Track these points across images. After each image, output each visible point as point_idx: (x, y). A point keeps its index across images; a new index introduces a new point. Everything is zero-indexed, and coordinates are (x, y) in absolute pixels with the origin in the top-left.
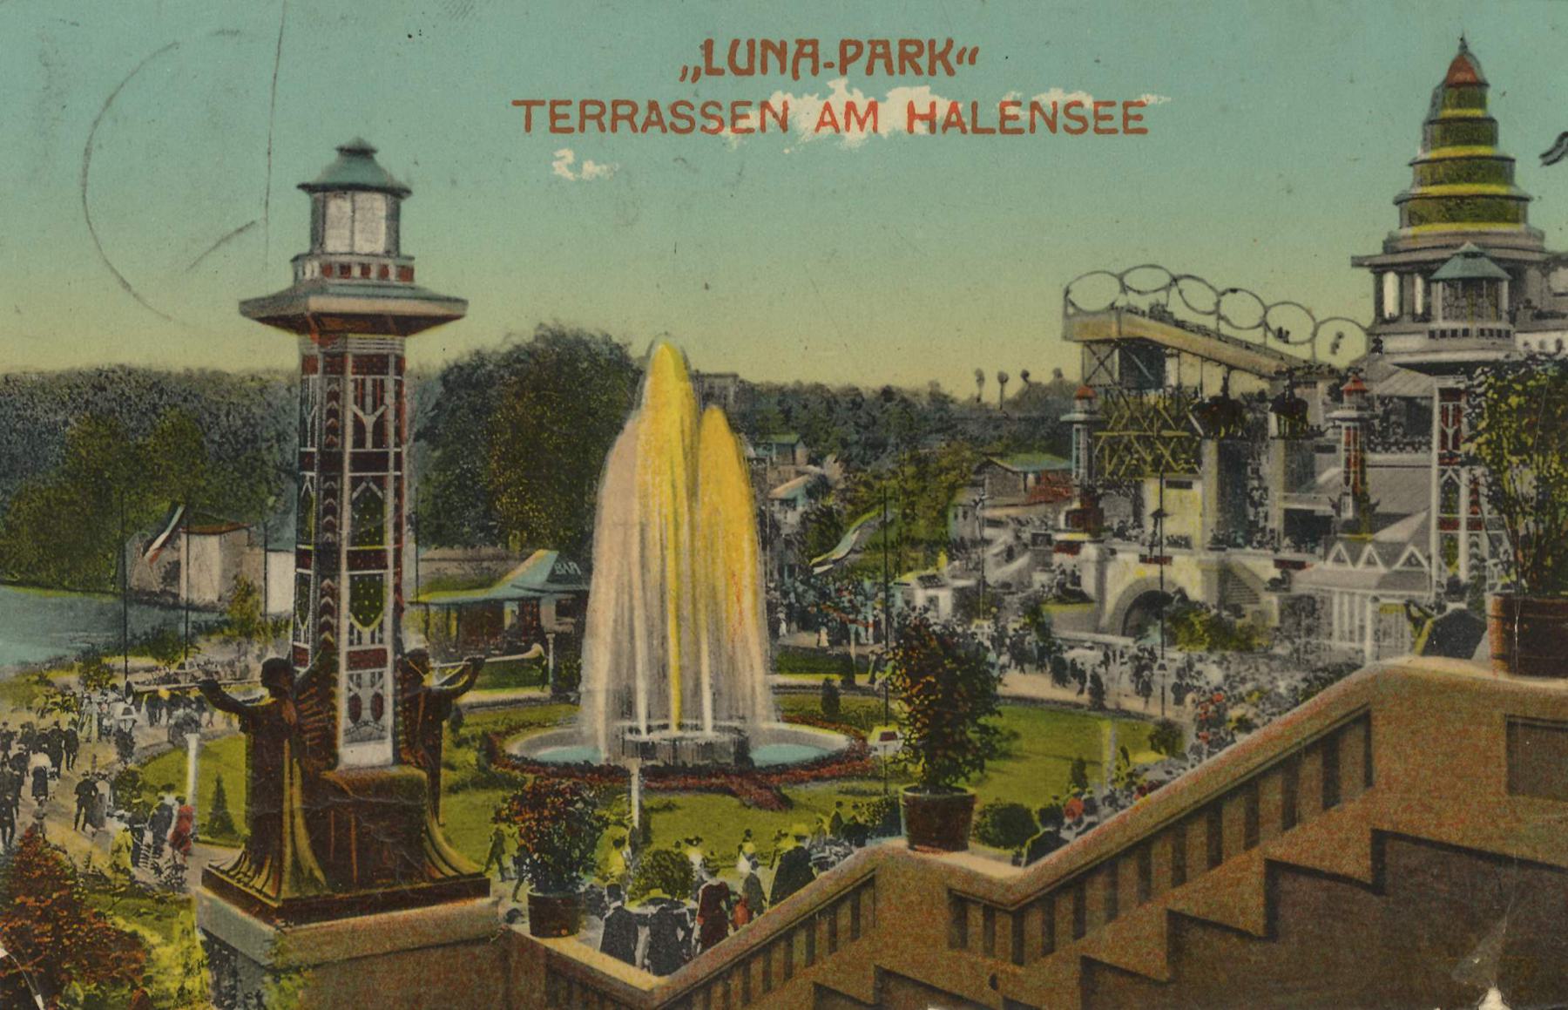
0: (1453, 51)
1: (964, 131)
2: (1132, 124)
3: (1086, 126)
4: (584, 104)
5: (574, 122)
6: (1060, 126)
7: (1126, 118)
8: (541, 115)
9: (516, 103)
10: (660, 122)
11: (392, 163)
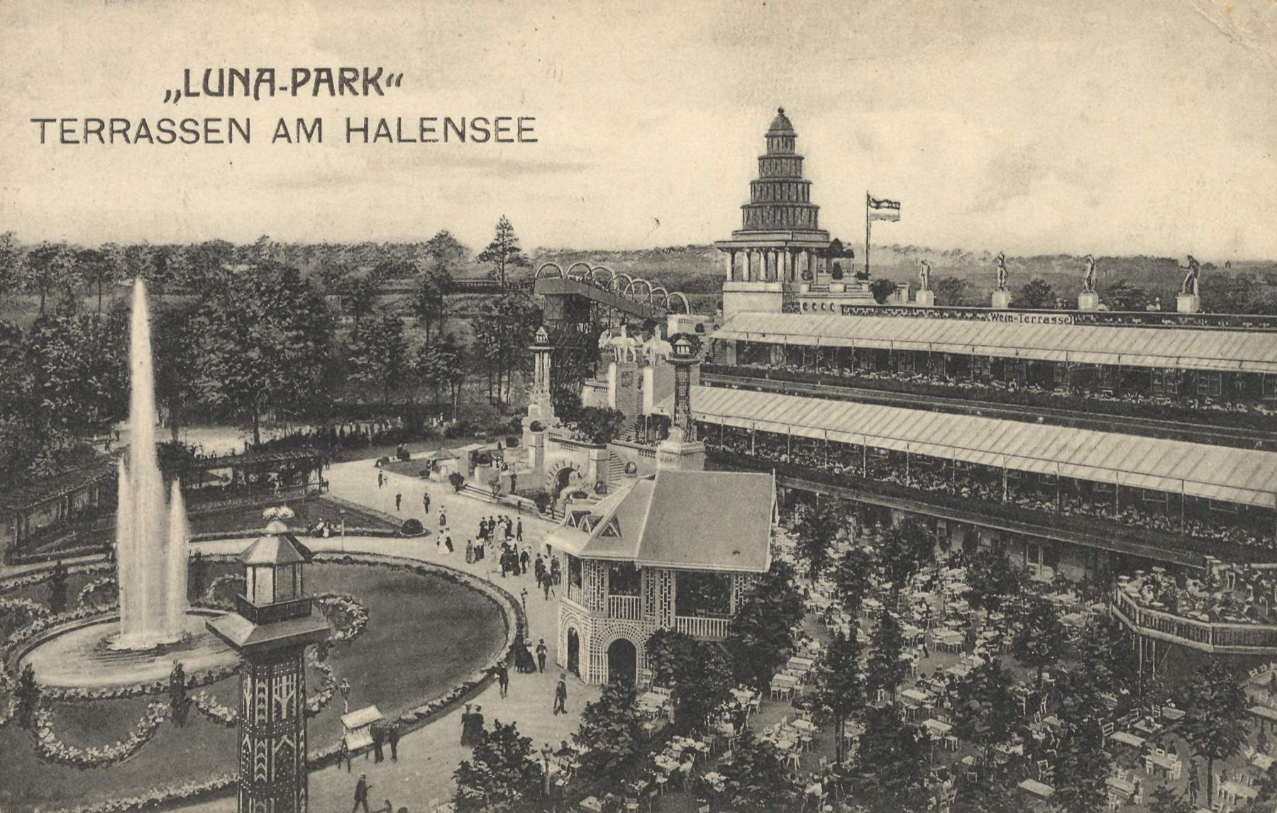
1: (290, 141)
3: (198, 138)
5: (79, 135)
7: (521, 130)
8: (53, 130)
10: (148, 136)
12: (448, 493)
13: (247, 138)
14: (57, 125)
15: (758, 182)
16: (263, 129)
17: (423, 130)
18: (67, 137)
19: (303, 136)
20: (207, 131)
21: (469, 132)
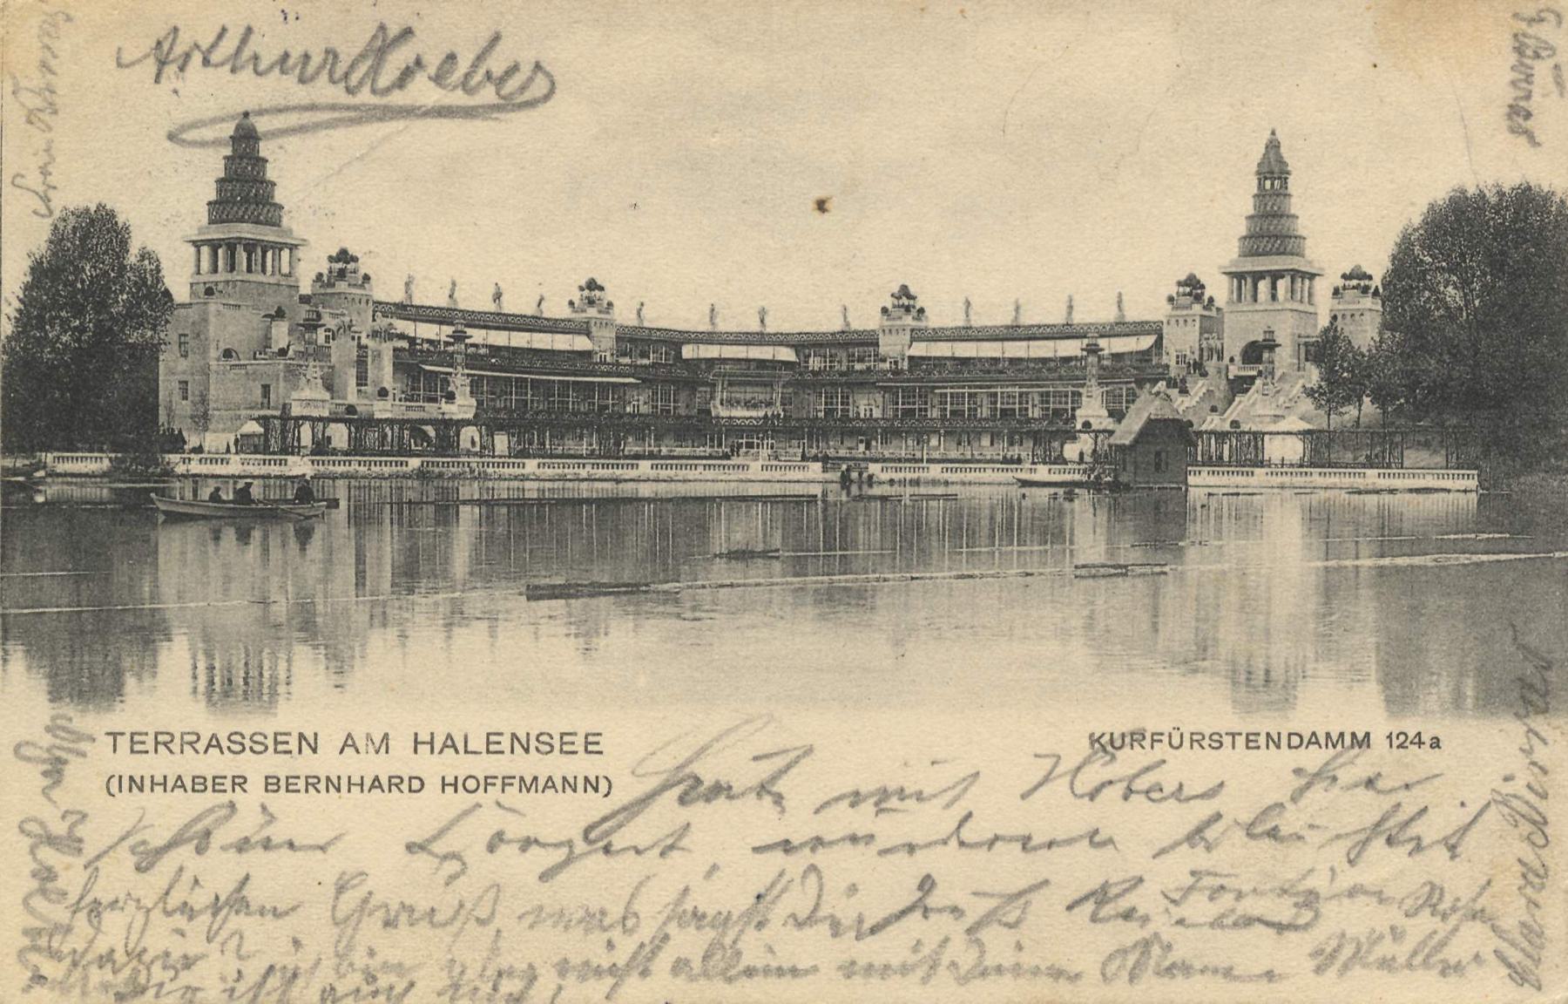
0: (1267, 135)
1: (457, 752)
2: (492, 748)
3: (267, 748)
4: (156, 734)
5: (150, 746)
6: (532, 749)
7: (587, 743)
8: (123, 742)
9: (416, 751)
10: (219, 746)
11: (912, 291)
12: (1181, 577)
13: (314, 751)
14: (128, 737)
15: (216, 202)
16: (401, 745)
17: (488, 743)
18: (137, 747)
19: (371, 749)
20: (276, 742)
21: (533, 743)
